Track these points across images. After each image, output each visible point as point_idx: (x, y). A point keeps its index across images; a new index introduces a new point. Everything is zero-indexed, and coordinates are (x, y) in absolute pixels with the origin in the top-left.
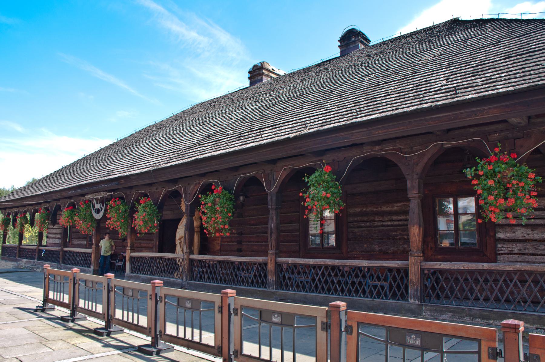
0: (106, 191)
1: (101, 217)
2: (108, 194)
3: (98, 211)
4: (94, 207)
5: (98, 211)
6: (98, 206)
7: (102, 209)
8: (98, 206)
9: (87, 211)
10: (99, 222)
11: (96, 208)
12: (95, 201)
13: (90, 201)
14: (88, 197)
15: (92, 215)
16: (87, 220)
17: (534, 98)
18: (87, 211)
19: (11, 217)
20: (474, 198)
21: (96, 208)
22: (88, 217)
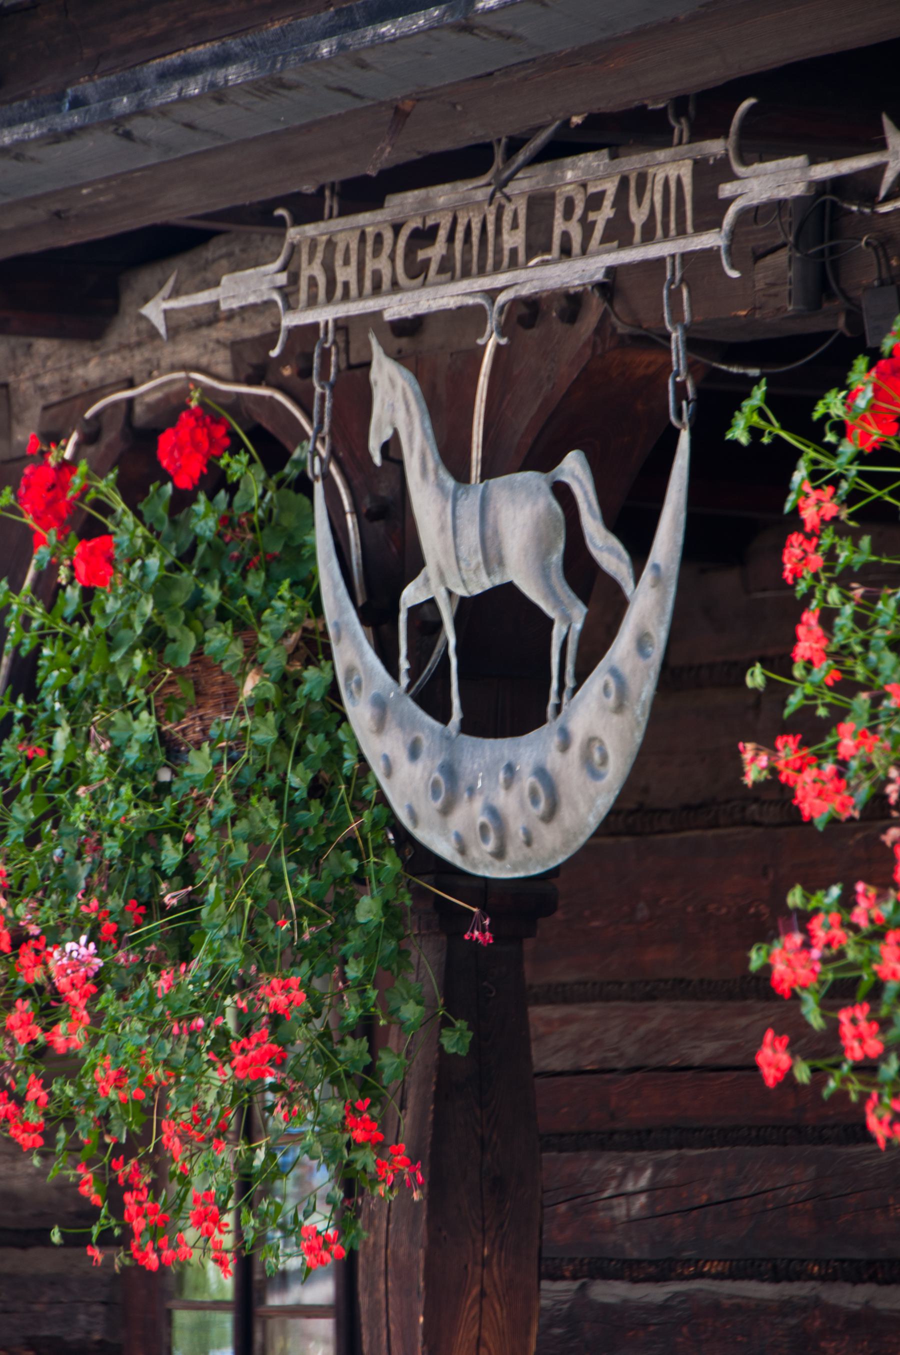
0: (705, 112)
1: (589, 803)
2: (772, 181)
3: (497, 670)
4: (387, 556)
5: (497, 670)
6: (486, 535)
7: (606, 606)
8: (486, 535)
9: (207, 684)
10: (485, 934)
11: (444, 578)
12: (396, 403)
13: (275, 422)
14: (178, 335)
15: (343, 783)
16: (221, 938)
17: (734, 370)
18: (207, 684)
19: (194, 90)
20: (463, 1053)
21: (444, 578)
22: (228, 841)
